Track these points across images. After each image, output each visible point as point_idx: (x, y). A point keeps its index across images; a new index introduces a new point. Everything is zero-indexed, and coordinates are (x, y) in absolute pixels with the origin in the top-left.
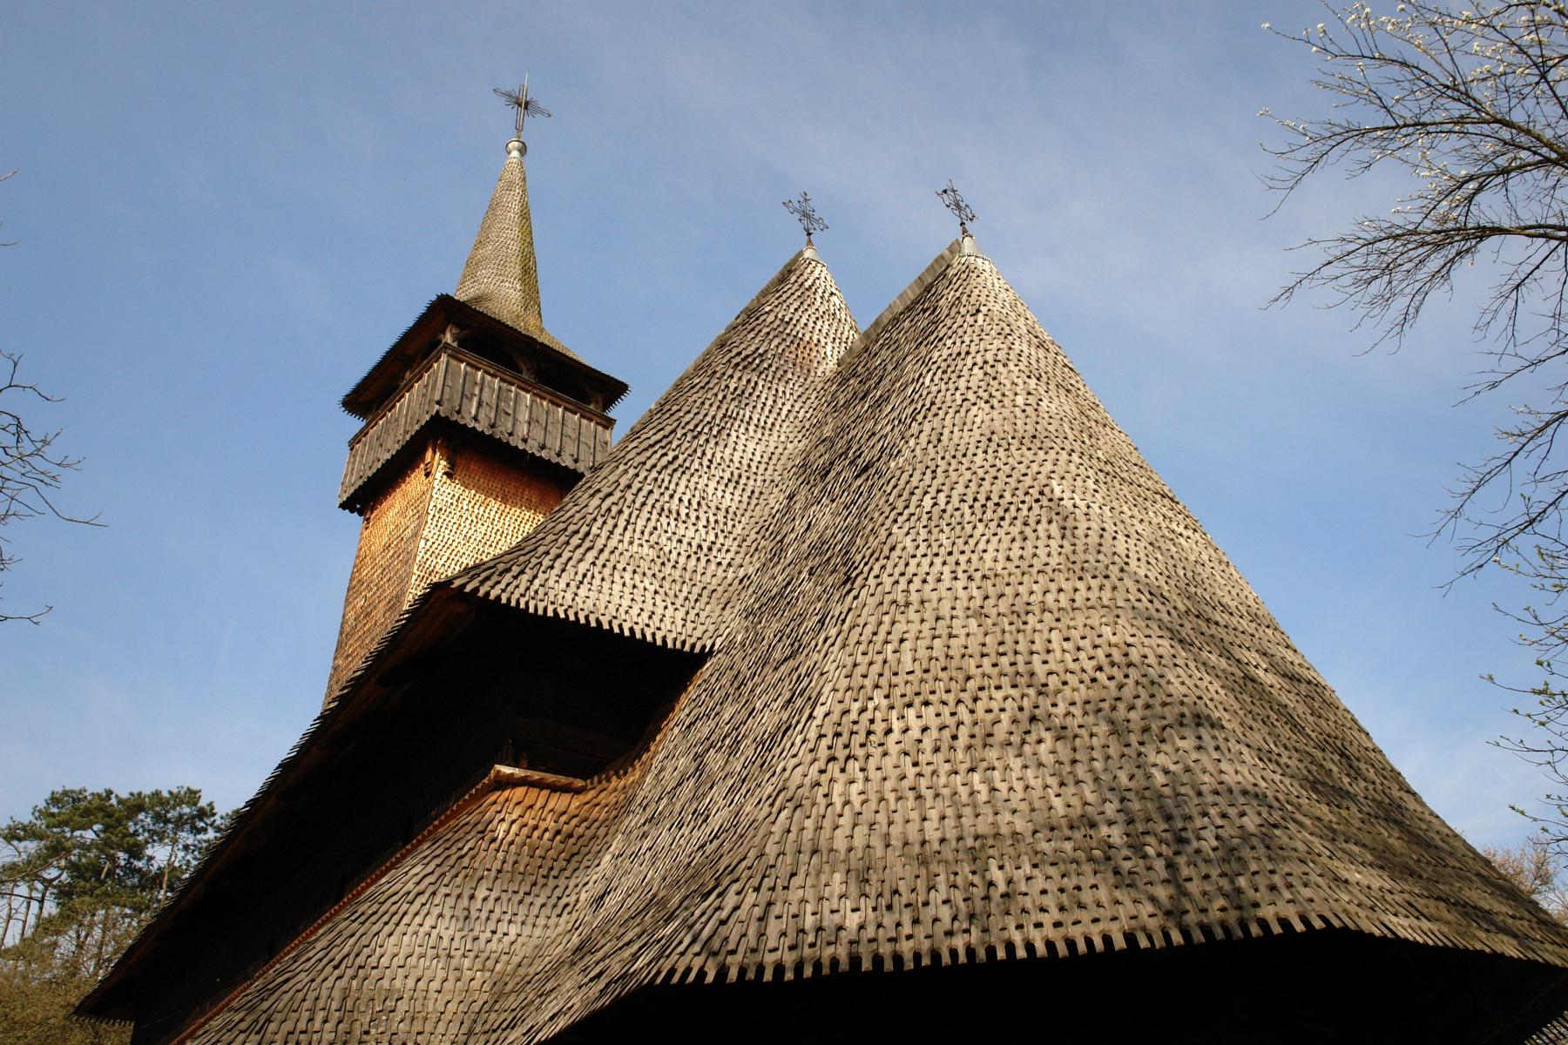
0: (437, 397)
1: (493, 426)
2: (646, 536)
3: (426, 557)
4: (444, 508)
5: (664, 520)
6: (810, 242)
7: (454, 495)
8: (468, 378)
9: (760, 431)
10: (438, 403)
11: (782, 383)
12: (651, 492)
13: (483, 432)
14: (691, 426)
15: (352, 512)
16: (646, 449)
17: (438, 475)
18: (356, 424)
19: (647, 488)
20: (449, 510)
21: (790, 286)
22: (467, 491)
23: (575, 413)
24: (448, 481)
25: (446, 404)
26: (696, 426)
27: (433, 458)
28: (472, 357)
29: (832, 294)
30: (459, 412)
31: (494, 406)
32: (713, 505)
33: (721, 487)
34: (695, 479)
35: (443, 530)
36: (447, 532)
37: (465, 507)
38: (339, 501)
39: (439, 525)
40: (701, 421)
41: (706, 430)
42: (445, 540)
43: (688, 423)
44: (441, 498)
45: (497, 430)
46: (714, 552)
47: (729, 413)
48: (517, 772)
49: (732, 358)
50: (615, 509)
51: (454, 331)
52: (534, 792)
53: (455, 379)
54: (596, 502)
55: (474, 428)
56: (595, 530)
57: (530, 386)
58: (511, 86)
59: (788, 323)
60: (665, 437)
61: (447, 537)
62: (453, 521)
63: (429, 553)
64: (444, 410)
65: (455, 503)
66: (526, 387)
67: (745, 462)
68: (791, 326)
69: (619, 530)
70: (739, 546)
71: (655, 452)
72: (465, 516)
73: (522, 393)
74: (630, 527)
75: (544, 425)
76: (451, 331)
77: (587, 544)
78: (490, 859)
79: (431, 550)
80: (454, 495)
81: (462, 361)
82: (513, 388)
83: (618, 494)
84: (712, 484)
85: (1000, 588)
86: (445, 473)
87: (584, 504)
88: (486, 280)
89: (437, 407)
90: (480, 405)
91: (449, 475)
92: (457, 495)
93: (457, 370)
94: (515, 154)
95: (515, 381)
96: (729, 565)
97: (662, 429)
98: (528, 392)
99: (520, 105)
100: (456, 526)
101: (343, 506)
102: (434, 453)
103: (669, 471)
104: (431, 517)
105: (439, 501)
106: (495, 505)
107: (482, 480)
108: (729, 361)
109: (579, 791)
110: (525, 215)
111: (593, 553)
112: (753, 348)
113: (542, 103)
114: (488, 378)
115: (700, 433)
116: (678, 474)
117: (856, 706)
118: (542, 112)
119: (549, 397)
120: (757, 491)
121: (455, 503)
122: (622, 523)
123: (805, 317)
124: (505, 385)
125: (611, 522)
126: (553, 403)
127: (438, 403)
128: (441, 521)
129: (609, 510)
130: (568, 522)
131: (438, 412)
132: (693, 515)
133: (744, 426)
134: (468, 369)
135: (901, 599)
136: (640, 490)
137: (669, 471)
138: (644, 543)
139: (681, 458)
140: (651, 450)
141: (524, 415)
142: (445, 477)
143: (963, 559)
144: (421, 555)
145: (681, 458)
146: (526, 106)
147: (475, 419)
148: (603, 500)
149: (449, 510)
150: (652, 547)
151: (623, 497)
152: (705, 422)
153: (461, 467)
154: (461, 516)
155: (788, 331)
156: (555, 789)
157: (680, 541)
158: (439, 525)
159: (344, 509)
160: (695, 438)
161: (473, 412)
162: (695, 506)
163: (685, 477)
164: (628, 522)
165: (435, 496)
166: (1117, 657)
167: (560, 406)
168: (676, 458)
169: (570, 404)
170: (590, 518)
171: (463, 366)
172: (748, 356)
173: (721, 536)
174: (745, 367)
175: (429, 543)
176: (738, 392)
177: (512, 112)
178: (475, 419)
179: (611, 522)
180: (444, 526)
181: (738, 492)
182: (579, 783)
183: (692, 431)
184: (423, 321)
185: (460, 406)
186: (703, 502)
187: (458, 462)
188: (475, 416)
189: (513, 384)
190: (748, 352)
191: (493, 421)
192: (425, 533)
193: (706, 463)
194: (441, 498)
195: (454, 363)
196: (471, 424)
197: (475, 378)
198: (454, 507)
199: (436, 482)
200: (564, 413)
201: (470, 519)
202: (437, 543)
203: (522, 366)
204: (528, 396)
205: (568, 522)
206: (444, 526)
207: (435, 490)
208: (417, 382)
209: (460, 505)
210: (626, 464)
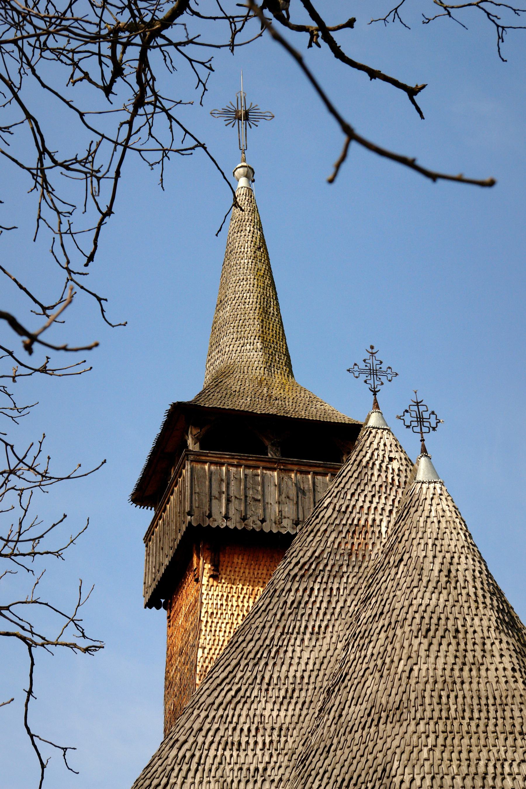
0: (187, 509)
1: (244, 519)
2: (213, 774)
3: (205, 666)
4: (215, 612)
5: (227, 753)
6: (376, 405)
7: (222, 595)
8: (213, 478)
9: (314, 637)
10: (190, 514)
11: (337, 580)
12: (218, 729)
13: (235, 528)
14: (252, 655)
15: (158, 608)
16: (215, 689)
17: (205, 581)
19: (215, 726)
20: (220, 612)
21: (350, 466)
22: (234, 587)
23: (325, 475)
24: (215, 583)
25: (196, 512)
26: (257, 653)
27: (198, 564)
29: (391, 459)
30: (210, 516)
31: (243, 497)
32: (268, 727)
33: (277, 707)
34: (254, 706)
35: (217, 633)
36: (222, 634)
37: (235, 604)
38: (143, 601)
39: (213, 629)
40: (261, 646)
41: (265, 655)
42: (221, 643)
43: (250, 652)
44: (211, 602)
45: (250, 522)
46: (268, 772)
47: (286, 630)
49: (290, 570)
50: (188, 755)
51: (195, 432)
55: (227, 527)
57: (275, 463)
59: (345, 512)
60: (230, 672)
61: (222, 639)
62: (225, 621)
63: (207, 661)
64: (196, 520)
65: (225, 603)
66: (272, 466)
67: (299, 675)
68: (347, 515)
69: (191, 774)
70: (289, 761)
71: (223, 689)
72: (236, 614)
73: (268, 472)
74: (201, 768)
75: (295, 500)
76: (191, 433)
79: (209, 657)
80: (222, 595)
81: (205, 462)
82: (259, 471)
83: (191, 740)
84: (269, 706)
86: (211, 576)
87: (165, 757)
88: (227, 349)
90: (228, 501)
92: (225, 595)
93: (202, 473)
95: (258, 463)
96: (281, 780)
97: (229, 664)
98: (273, 469)
100: (229, 626)
101: (149, 605)
102: (199, 558)
103: (232, 706)
104: (204, 624)
105: (210, 606)
107: (247, 571)
108: (288, 574)
112: (309, 554)
114: (233, 470)
115: (260, 659)
116: (240, 706)
119: (296, 468)
120: (308, 700)
121: (225, 603)
122: (194, 766)
123: (362, 498)
124: (249, 471)
125: (185, 767)
126: (301, 472)
128: (214, 625)
129: (184, 756)
130: (152, 778)
131: (190, 523)
132: (252, 741)
133: (300, 637)
134: (213, 468)
136: (209, 730)
137: (232, 706)
138: (211, 779)
139: (244, 688)
140: (219, 689)
141: (273, 495)
142: (211, 580)
144: (200, 664)
145: (244, 688)
147: (227, 517)
148: (180, 749)
149: (220, 612)
150: (218, 781)
151: (195, 741)
152: (265, 646)
153: (225, 564)
154: (233, 614)
155: (344, 522)
157: (241, 769)
158: (213, 629)
159: (151, 608)
160: (255, 665)
161: (223, 510)
162: (253, 733)
163: (247, 706)
164: (199, 764)
165: (205, 602)
167: (309, 473)
168: (239, 689)
169: (319, 467)
170: (169, 768)
171: (206, 467)
172: (305, 564)
173: (275, 754)
174: (303, 576)
175: (206, 651)
176: (295, 605)
178: (227, 517)
179: (185, 767)
180: (218, 629)
181: (291, 707)
183: (254, 659)
184: (168, 426)
185: (210, 510)
186: (260, 726)
187: (222, 559)
189: (258, 468)
190: (306, 559)
191: (243, 514)
192: (201, 641)
194: (211, 602)
195: (198, 466)
197: (221, 474)
198: (224, 607)
199: (204, 588)
200: (313, 479)
201: (241, 614)
202: (214, 648)
204: (276, 474)
205: (152, 778)
206: (218, 629)
207: (204, 596)
208: (176, 486)
209: (230, 604)
210: (198, 709)
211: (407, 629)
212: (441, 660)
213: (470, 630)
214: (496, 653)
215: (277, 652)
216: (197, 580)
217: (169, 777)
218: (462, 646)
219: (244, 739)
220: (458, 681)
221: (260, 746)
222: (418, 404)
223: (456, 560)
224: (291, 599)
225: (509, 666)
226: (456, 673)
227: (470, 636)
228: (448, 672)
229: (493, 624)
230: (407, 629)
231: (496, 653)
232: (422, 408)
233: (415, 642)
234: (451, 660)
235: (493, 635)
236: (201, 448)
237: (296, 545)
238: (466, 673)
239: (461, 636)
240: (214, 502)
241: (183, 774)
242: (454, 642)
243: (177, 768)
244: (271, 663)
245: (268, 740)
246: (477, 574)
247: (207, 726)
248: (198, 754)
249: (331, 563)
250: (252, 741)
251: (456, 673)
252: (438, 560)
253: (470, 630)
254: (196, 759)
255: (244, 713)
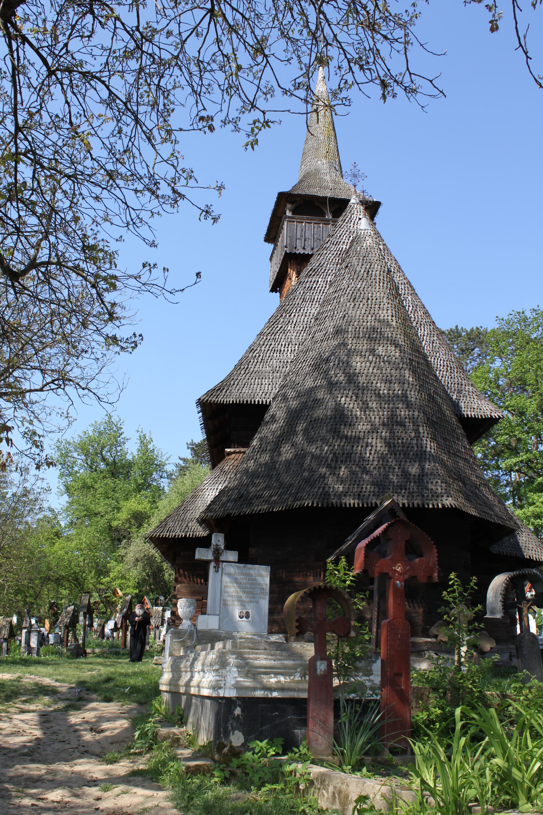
5: (275, 355)
10: (286, 247)
19: (269, 343)
30: (296, 248)
32: (294, 343)
48: (232, 450)
50: (257, 355)
52: (238, 455)
56: (250, 366)
58: (382, 101)
69: (258, 364)
77: (247, 371)
110: (340, 161)
111: (249, 375)
114: (307, 225)
127: (286, 247)
132: (286, 349)
179: (256, 361)
193: (293, 325)
211: (345, 298)
212: (358, 312)
213: (375, 298)
214: (385, 309)
215: (300, 310)
216: (290, 279)
217: (248, 365)
218: (370, 306)
219: (283, 349)
220: (365, 321)
221: (290, 351)
222: (363, 192)
223: (372, 267)
224: (308, 286)
225: (390, 314)
226: (365, 317)
227: (374, 301)
228: (361, 317)
229: (386, 296)
230: (345, 298)
231: (385, 309)
232: (365, 194)
233: (348, 304)
234: (363, 312)
235: (385, 301)
236: (293, 214)
237: (312, 260)
238: (369, 318)
239: (369, 301)
240: (298, 241)
241: (254, 364)
242: (366, 304)
243: (252, 361)
244: (297, 315)
245: (293, 349)
246: (382, 273)
247: (266, 343)
248: (261, 355)
249: (327, 269)
250: (286, 349)
251: (365, 317)
252: (364, 267)
253: (375, 298)
254: (261, 357)
255: (283, 337)
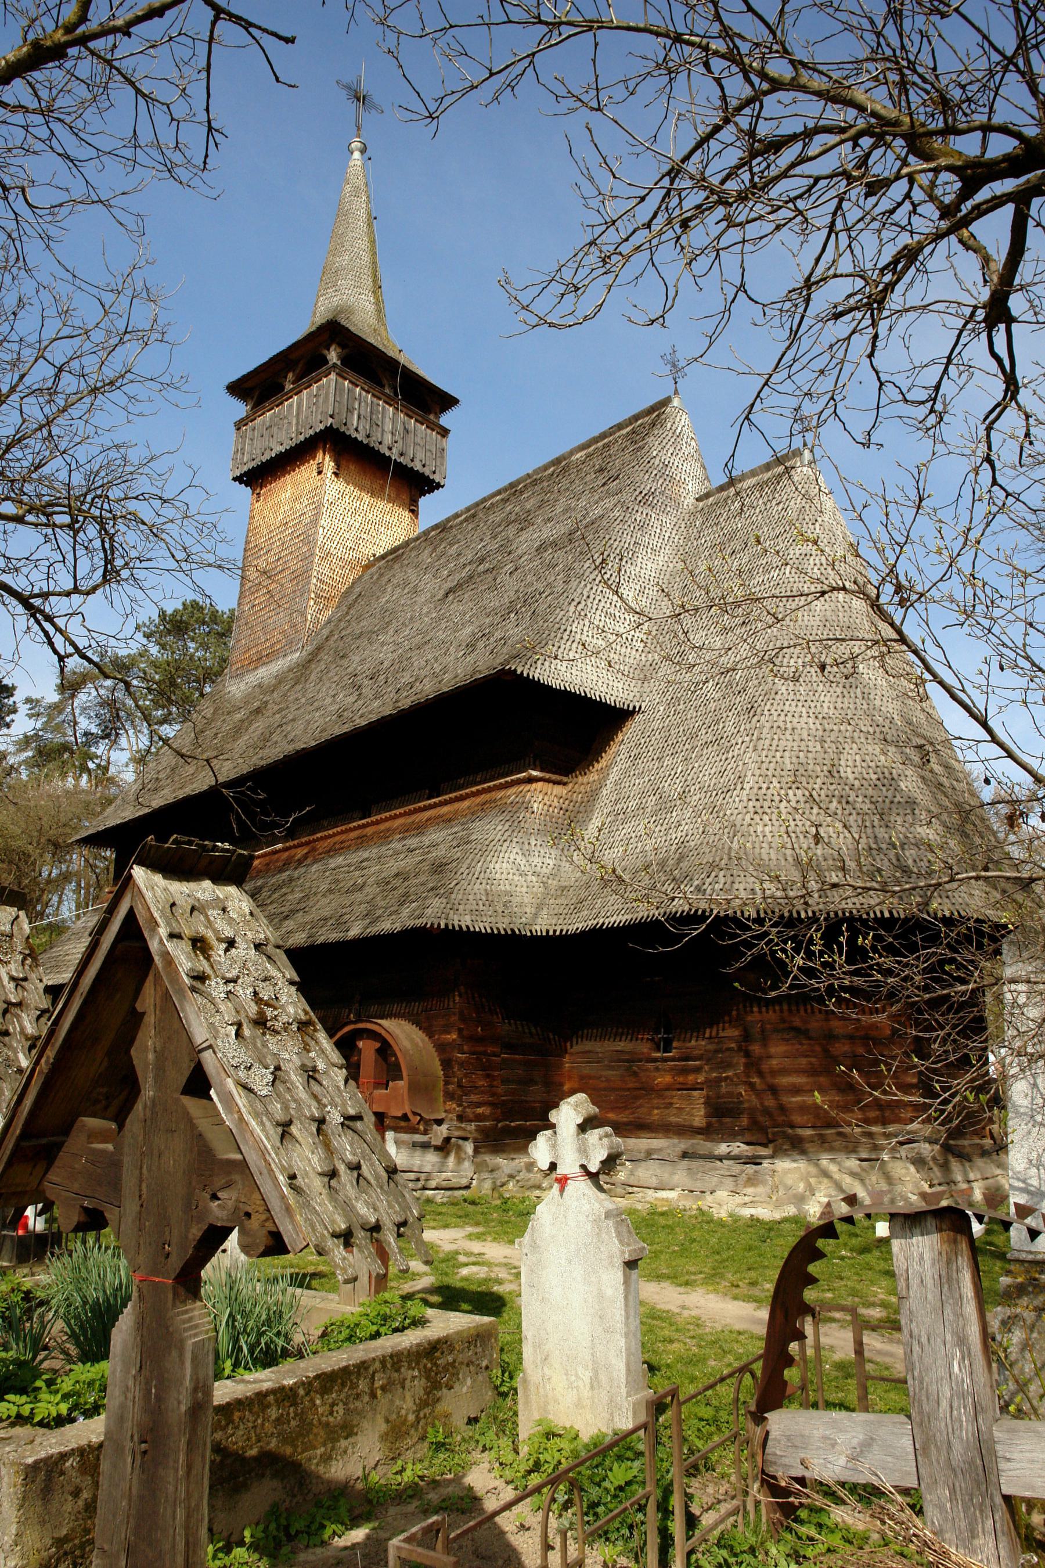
1: (368, 436)
10: (331, 416)
18: (240, 409)
28: (352, 376)
51: (339, 350)
53: (341, 395)
54: (572, 609)
78: (532, 822)
85: (831, 726)
89: (330, 420)
91: (336, 474)
94: (357, 155)
99: (358, 100)
101: (238, 479)
106: (367, 498)
109: (565, 784)
113: (376, 97)
117: (765, 786)
118: (375, 107)
135: (782, 725)
143: (813, 705)
146: (360, 98)
147: (356, 430)
156: (555, 783)
166: (887, 775)
177: (351, 106)
182: (565, 779)
184: (310, 337)
188: (357, 428)
195: (340, 380)
196: (354, 435)
203: (385, 381)
